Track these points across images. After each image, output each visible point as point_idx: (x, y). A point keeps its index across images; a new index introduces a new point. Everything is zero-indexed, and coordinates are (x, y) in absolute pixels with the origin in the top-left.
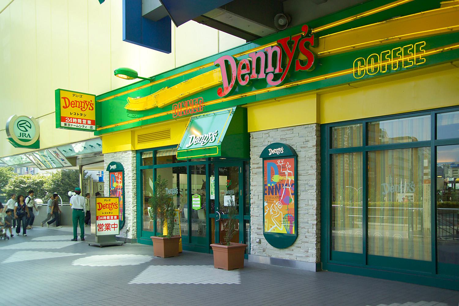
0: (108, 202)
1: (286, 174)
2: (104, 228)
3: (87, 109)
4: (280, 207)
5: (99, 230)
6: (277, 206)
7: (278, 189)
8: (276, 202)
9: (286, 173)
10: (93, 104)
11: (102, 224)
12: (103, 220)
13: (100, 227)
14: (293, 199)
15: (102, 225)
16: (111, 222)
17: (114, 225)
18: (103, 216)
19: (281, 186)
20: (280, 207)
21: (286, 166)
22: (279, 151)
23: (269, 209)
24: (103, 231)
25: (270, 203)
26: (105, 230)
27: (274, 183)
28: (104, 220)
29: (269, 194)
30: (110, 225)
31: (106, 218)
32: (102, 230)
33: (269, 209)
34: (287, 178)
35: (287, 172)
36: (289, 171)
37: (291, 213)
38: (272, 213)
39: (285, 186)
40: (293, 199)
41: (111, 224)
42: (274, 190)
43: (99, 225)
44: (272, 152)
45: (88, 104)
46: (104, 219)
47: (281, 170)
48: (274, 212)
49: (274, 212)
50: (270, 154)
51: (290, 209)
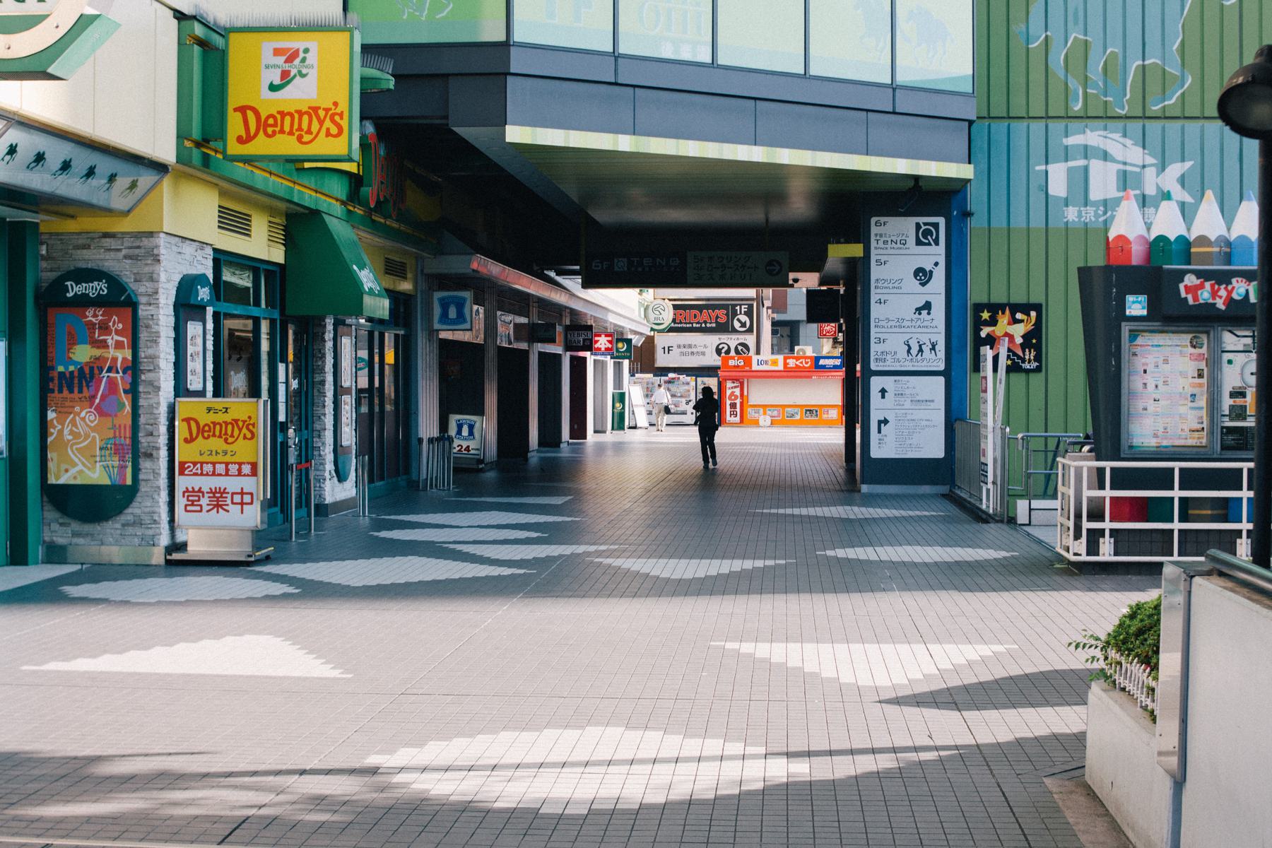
0: (220, 418)
1: (110, 344)
2: (204, 501)
3: (318, 138)
4: (92, 422)
5: (189, 508)
6: (83, 419)
7: (85, 377)
8: (81, 412)
9: (110, 342)
10: (341, 115)
11: (196, 489)
12: (202, 474)
13: (190, 498)
14: (127, 403)
15: (200, 490)
16: (232, 484)
17: (242, 493)
18: (202, 463)
19: (96, 371)
20: (92, 422)
21: (111, 324)
22: (97, 288)
23: (60, 427)
24: (201, 511)
25: (63, 413)
26: (208, 511)
27: (75, 363)
28: (207, 475)
29: (61, 391)
30: (224, 495)
31: (214, 471)
32: (198, 508)
33: (60, 427)
34: (112, 352)
35: (112, 339)
36: (117, 338)
37: (123, 436)
38: (70, 437)
39: (107, 372)
40: (127, 403)
41: (230, 490)
42: (76, 381)
43: (187, 491)
44: (76, 289)
45: (325, 117)
46: (205, 473)
47: (95, 333)
48: (76, 435)
49: (76, 435)
50: (68, 295)
51: (120, 426)
